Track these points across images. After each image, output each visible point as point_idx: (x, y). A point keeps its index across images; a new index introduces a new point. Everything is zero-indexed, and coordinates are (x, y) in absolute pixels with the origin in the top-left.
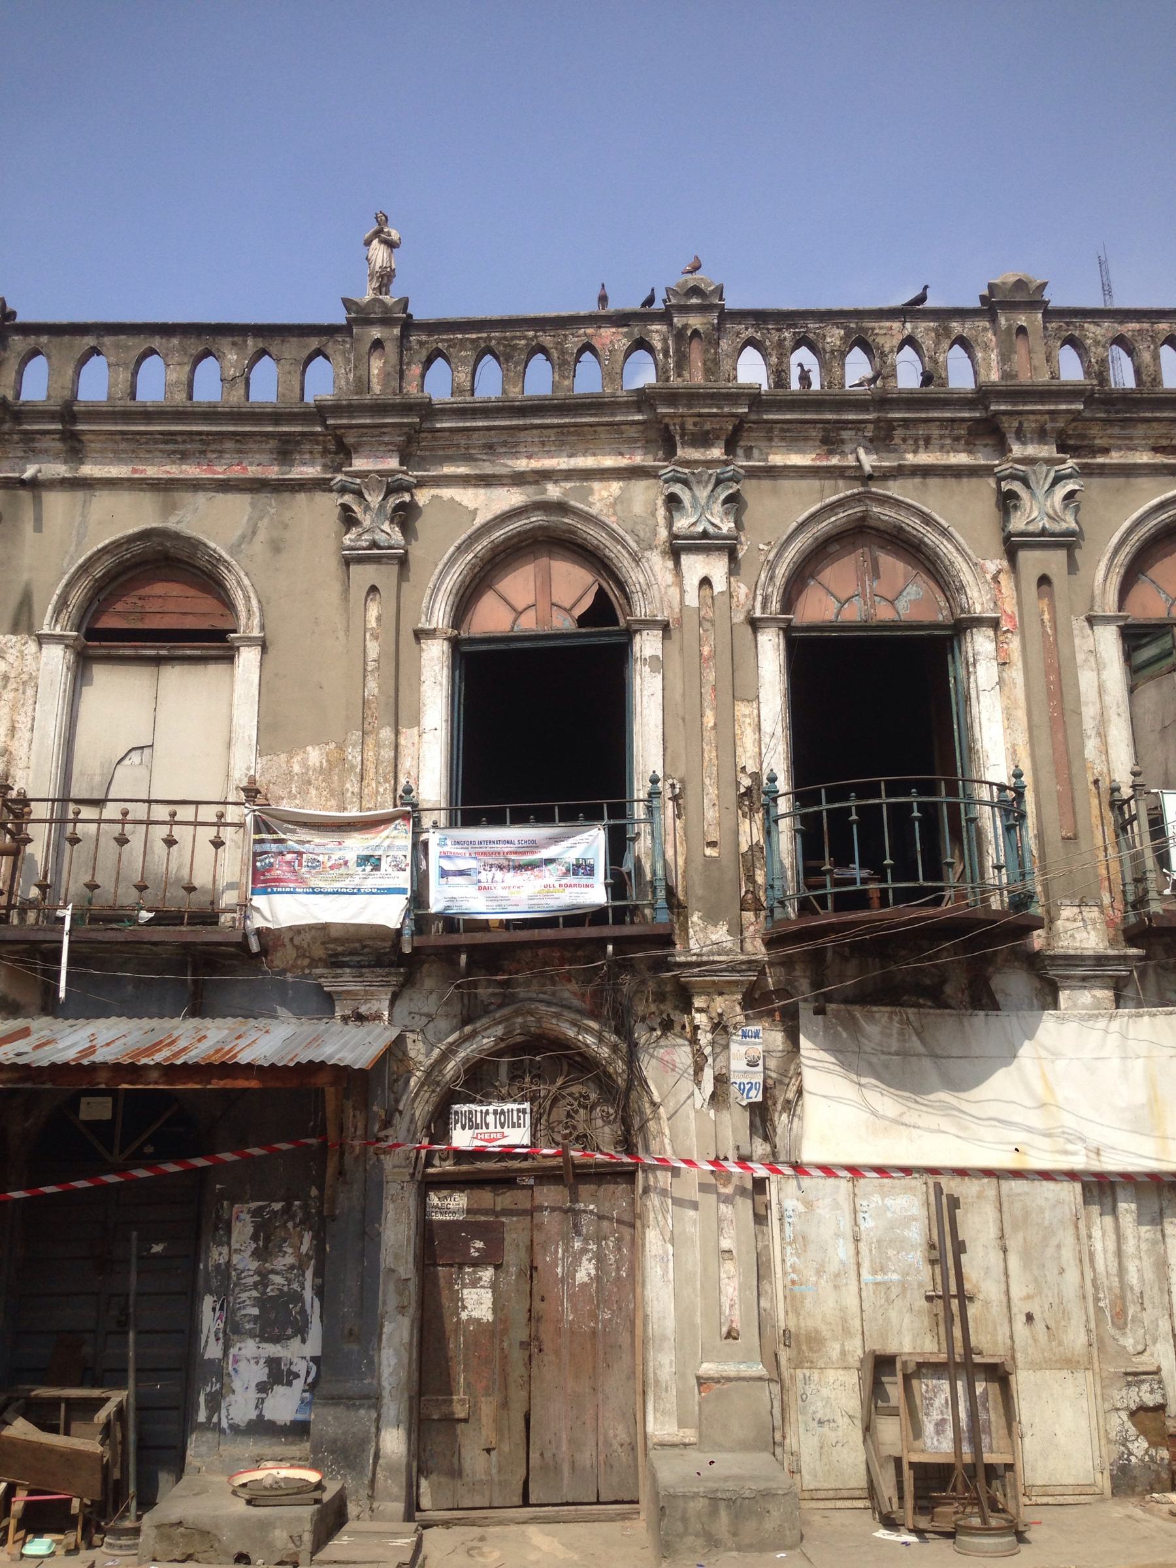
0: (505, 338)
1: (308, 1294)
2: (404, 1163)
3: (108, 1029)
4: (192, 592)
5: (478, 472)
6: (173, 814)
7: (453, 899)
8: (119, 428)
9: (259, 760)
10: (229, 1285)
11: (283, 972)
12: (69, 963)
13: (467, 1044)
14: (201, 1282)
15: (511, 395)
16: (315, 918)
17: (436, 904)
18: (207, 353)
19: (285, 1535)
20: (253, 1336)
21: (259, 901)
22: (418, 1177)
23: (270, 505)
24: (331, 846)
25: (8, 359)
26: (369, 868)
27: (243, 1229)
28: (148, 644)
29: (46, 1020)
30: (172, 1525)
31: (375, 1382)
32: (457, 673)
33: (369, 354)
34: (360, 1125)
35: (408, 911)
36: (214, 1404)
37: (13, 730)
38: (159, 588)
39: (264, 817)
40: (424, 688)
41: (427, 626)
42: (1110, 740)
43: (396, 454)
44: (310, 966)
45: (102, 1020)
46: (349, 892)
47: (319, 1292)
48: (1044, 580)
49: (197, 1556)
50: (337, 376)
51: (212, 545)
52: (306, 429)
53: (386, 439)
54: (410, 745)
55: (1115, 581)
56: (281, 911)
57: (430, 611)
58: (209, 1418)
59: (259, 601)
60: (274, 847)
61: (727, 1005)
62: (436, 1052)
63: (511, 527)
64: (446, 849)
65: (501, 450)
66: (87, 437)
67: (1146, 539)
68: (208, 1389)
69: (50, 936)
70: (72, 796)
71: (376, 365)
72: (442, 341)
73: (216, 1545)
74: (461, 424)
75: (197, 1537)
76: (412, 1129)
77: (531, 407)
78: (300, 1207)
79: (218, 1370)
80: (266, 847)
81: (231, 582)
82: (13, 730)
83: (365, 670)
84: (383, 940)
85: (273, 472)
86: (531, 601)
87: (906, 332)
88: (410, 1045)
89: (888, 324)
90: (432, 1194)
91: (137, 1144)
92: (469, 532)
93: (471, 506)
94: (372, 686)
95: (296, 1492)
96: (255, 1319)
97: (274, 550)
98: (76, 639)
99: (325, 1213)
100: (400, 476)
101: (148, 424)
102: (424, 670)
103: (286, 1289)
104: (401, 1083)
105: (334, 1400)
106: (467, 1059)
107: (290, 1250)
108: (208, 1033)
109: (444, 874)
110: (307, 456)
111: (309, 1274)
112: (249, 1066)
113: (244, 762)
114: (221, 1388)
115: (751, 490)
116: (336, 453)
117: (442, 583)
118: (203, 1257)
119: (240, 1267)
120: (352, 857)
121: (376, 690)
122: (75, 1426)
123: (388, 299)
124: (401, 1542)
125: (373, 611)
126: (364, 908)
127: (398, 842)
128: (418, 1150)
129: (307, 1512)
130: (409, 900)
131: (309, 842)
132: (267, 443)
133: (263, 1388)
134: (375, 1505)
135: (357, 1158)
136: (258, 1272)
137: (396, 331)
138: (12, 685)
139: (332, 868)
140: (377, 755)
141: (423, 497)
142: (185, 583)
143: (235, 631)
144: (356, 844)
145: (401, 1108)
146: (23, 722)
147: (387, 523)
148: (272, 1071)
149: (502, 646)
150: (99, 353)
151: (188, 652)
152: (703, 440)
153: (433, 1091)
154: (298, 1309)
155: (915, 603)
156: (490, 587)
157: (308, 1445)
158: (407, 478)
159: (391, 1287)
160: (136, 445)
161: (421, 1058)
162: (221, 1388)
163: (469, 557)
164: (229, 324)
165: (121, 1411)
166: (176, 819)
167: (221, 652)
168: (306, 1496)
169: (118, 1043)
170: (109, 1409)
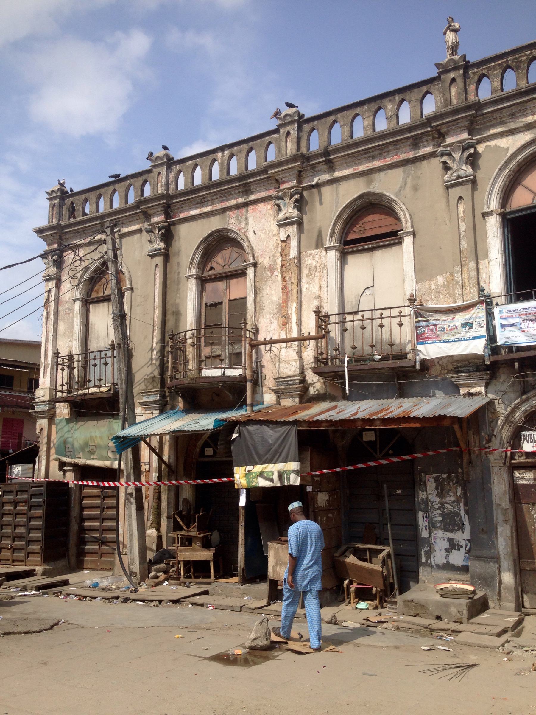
0: (516, 59)
1: (462, 513)
2: (499, 458)
3: (366, 404)
4: (383, 217)
5: (507, 129)
6: (401, 312)
7: (509, 338)
8: (346, 153)
9: (417, 286)
10: (428, 508)
11: (436, 377)
12: (349, 380)
13: (525, 404)
14: (417, 507)
15: (521, 86)
16: (446, 353)
17: (500, 341)
18: (380, 108)
19: (455, 610)
20: (442, 529)
21: (420, 347)
22: (507, 464)
23: (411, 170)
24: (449, 320)
25: (303, 135)
26: (467, 328)
27: (431, 485)
28: (367, 243)
29: (344, 402)
30: (409, 601)
31: (496, 552)
32: (506, 230)
33: (450, 86)
34: (477, 442)
35: (487, 345)
36: (428, 554)
37: (320, 288)
38: (370, 218)
39: (419, 311)
41: (488, 210)
43: (466, 131)
44: (447, 373)
45: (365, 401)
47: (467, 512)
49: (420, 615)
50: (436, 102)
51: (388, 194)
52: (423, 131)
53: (460, 125)
54: (484, 268)
56: (431, 351)
57: (489, 202)
58: (427, 561)
59: (410, 215)
60: (424, 324)
62: (509, 409)
63: (527, 152)
64: (503, 315)
65: (519, 115)
66: (335, 160)
68: (425, 549)
69: (340, 369)
70: (345, 311)
71: (454, 91)
72: (484, 69)
73: (428, 611)
74: (496, 108)
75: (419, 607)
76: (502, 443)
77: (531, 89)
78: (455, 476)
79: (428, 542)
80: (421, 324)
81: (397, 209)
82: (320, 288)
83: (460, 237)
84: (478, 359)
85: (411, 155)
88: (497, 405)
90: (516, 472)
91: (386, 450)
92: (505, 160)
93: (506, 147)
95: (462, 593)
96: (441, 522)
97: (415, 190)
98: (339, 246)
99: (465, 479)
100: (468, 141)
101: (358, 148)
102: (488, 232)
103: (452, 510)
104: (494, 422)
105: (478, 558)
106: (526, 411)
107: (452, 494)
108: (404, 405)
109: (503, 326)
110: (426, 143)
111: (462, 504)
112: (414, 418)
113: (410, 287)
114: (430, 549)
116: (439, 138)
117: (494, 187)
118: (416, 495)
119: (432, 500)
120: (458, 324)
121: (466, 245)
122: (374, 560)
123: (456, 57)
124: (510, 619)
125: (461, 208)
126: (467, 346)
127: (480, 315)
128: (506, 452)
129: (464, 602)
130: (487, 340)
131: (439, 320)
132: (407, 142)
133: (447, 550)
134: (501, 603)
135: (477, 456)
136: (440, 503)
137: (461, 71)
138: (318, 270)
139: (450, 330)
140: (469, 275)
141: (481, 148)
142: (380, 213)
143: (402, 230)
144: (460, 318)
145: (495, 434)
146: (324, 283)
147: (464, 165)
148: (424, 419)
149: (528, 212)
150: (337, 122)
151: (384, 243)
153: (510, 426)
154: (459, 519)
156: (519, 184)
157: (469, 575)
158: (471, 141)
159: (499, 511)
160: (354, 159)
161: (503, 411)
162: (430, 549)
163: (507, 172)
164: (390, 92)
165: (389, 555)
166: (402, 314)
167: (397, 241)
168: (466, 596)
169: (367, 410)
170: (384, 553)
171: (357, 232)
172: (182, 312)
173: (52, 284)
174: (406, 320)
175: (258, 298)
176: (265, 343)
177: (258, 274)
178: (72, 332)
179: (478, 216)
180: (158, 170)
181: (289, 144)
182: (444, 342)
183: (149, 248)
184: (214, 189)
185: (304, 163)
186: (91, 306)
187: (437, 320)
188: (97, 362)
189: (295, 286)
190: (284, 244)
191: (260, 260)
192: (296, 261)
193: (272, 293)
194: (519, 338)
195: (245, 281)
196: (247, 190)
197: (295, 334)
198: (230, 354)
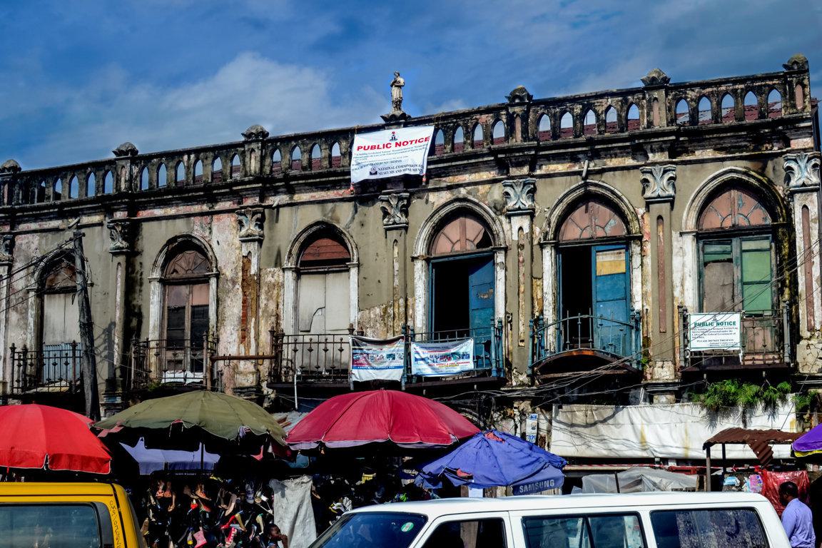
0: (445, 124)
17: (414, 371)
46: (383, 366)
48: (660, 218)
55: (694, 214)
60: (359, 352)
61: (525, 405)
67: (712, 191)
80: (357, 351)
86: (458, 238)
87: (609, 104)
89: (601, 100)
94: (397, 281)
109: (416, 360)
113: (354, 316)
115: (540, 184)
120: (385, 355)
125: (396, 250)
127: (400, 349)
144: (387, 350)
151: (335, 269)
152: (519, 165)
171: (313, 255)
172: (144, 313)
174: (345, 346)
175: (220, 309)
176: (224, 358)
177: (220, 285)
178: (26, 324)
179: (409, 259)
181: (253, 161)
182: (374, 368)
185: (267, 184)
186: (45, 296)
187: (369, 350)
188: (57, 361)
190: (245, 260)
191: (224, 271)
193: (234, 307)
196: (213, 200)
197: (252, 353)
198: (192, 360)
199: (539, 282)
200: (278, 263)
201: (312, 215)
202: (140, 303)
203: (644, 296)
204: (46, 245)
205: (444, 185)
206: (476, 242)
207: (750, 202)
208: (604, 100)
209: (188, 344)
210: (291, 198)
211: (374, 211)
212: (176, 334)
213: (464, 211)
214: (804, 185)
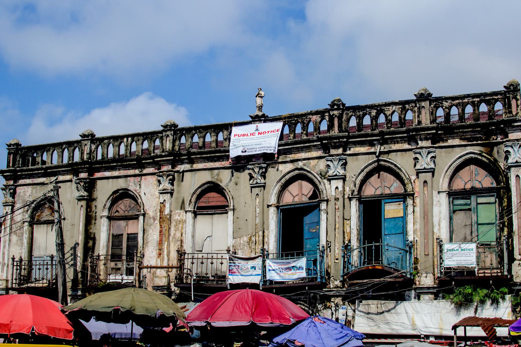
40: (270, 220)
42: (441, 227)
46: (248, 274)
48: (425, 182)
55: (447, 180)
61: (339, 300)
94: (258, 220)
109: (269, 270)
113: (230, 242)
120: (249, 267)
125: (258, 200)
144: (251, 263)
152: (336, 147)
155: (396, 188)
171: (205, 202)
172: (97, 236)
173: (8, 209)
175: (145, 236)
176: (147, 267)
177: (146, 221)
179: (266, 206)
180: (86, 142)
181: (168, 142)
183: (77, 194)
184: (120, 162)
188: (41, 267)
189: (167, 232)
190: (162, 205)
191: (148, 212)
192: (168, 217)
193: (154, 235)
194: (276, 278)
195: (138, 223)
197: (165, 264)
199: (348, 222)
200: (182, 207)
201: (205, 177)
202: (94, 231)
203: (415, 231)
204: (36, 193)
205: (288, 159)
206: (309, 196)
207: (483, 173)
208: (390, 107)
209: (124, 258)
210: (192, 166)
211: (244, 176)
212: (117, 251)
213: (301, 176)
214: (517, 162)
